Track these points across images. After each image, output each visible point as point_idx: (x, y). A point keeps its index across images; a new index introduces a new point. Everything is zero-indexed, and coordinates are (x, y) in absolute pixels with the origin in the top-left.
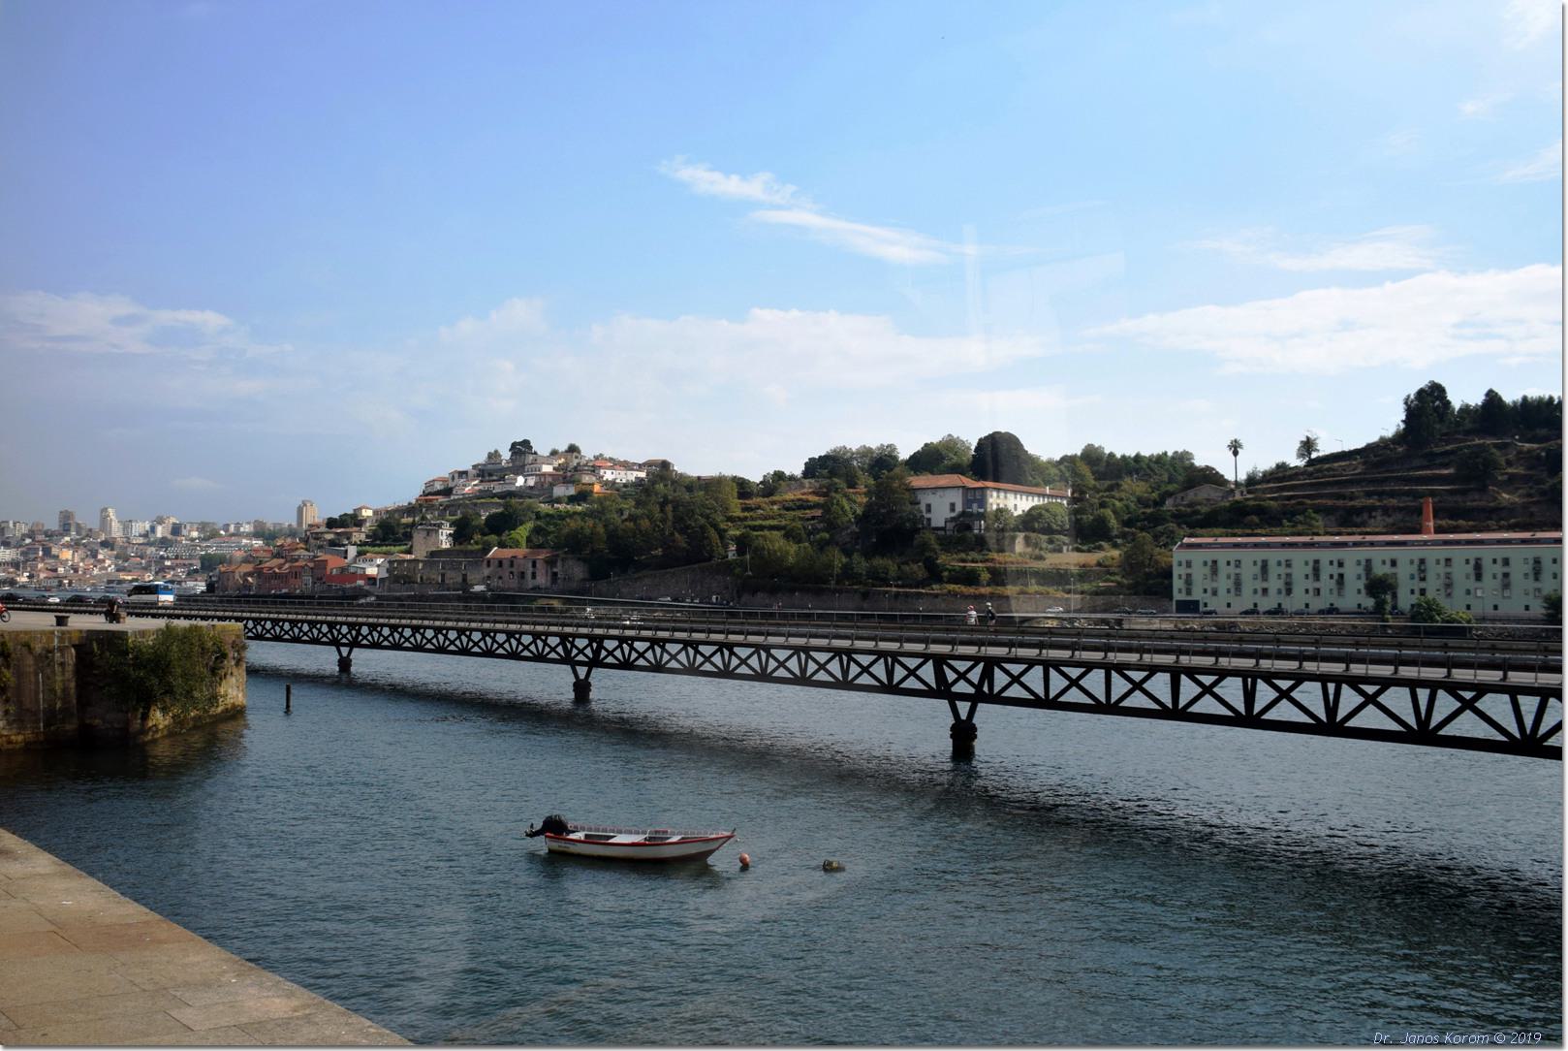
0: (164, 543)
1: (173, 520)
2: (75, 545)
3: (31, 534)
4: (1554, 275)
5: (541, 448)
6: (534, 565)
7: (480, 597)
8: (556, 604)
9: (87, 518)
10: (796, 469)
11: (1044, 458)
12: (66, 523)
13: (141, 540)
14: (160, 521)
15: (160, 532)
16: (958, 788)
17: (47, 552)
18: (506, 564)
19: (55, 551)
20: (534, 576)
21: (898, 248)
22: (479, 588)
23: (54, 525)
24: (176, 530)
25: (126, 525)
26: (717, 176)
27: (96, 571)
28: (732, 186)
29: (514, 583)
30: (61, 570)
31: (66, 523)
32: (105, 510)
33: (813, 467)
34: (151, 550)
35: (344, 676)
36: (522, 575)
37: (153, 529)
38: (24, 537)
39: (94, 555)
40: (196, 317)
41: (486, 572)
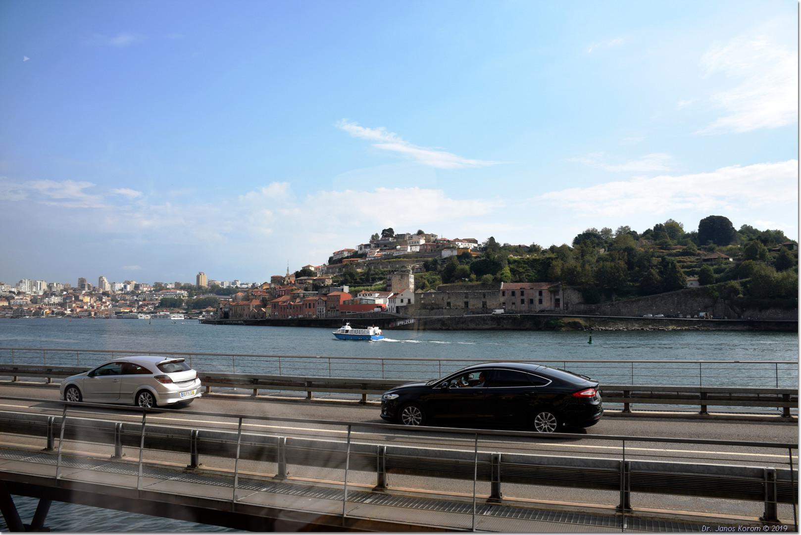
0: (132, 293)
1: (134, 282)
2: (90, 294)
3: (65, 290)
4: (794, 166)
6: (541, 293)
7: (498, 319)
8: (582, 322)
9: (92, 282)
10: (652, 228)
12: (82, 284)
13: (120, 292)
14: (129, 283)
15: (129, 288)
16: (241, 418)
17: (77, 298)
18: (518, 294)
19: (81, 298)
20: (541, 302)
21: (437, 159)
22: (500, 311)
23: (75, 285)
24: (137, 287)
25: (113, 285)
26: (360, 128)
27: (103, 308)
28: (367, 133)
29: (525, 307)
30: (85, 307)
31: (82, 284)
32: (101, 278)
33: (579, 240)
34: (127, 297)
35: (704, 404)
36: (532, 301)
37: (125, 287)
38: (62, 291)
39: (101, 300)
40: (123, 191)
41: (502, 299)
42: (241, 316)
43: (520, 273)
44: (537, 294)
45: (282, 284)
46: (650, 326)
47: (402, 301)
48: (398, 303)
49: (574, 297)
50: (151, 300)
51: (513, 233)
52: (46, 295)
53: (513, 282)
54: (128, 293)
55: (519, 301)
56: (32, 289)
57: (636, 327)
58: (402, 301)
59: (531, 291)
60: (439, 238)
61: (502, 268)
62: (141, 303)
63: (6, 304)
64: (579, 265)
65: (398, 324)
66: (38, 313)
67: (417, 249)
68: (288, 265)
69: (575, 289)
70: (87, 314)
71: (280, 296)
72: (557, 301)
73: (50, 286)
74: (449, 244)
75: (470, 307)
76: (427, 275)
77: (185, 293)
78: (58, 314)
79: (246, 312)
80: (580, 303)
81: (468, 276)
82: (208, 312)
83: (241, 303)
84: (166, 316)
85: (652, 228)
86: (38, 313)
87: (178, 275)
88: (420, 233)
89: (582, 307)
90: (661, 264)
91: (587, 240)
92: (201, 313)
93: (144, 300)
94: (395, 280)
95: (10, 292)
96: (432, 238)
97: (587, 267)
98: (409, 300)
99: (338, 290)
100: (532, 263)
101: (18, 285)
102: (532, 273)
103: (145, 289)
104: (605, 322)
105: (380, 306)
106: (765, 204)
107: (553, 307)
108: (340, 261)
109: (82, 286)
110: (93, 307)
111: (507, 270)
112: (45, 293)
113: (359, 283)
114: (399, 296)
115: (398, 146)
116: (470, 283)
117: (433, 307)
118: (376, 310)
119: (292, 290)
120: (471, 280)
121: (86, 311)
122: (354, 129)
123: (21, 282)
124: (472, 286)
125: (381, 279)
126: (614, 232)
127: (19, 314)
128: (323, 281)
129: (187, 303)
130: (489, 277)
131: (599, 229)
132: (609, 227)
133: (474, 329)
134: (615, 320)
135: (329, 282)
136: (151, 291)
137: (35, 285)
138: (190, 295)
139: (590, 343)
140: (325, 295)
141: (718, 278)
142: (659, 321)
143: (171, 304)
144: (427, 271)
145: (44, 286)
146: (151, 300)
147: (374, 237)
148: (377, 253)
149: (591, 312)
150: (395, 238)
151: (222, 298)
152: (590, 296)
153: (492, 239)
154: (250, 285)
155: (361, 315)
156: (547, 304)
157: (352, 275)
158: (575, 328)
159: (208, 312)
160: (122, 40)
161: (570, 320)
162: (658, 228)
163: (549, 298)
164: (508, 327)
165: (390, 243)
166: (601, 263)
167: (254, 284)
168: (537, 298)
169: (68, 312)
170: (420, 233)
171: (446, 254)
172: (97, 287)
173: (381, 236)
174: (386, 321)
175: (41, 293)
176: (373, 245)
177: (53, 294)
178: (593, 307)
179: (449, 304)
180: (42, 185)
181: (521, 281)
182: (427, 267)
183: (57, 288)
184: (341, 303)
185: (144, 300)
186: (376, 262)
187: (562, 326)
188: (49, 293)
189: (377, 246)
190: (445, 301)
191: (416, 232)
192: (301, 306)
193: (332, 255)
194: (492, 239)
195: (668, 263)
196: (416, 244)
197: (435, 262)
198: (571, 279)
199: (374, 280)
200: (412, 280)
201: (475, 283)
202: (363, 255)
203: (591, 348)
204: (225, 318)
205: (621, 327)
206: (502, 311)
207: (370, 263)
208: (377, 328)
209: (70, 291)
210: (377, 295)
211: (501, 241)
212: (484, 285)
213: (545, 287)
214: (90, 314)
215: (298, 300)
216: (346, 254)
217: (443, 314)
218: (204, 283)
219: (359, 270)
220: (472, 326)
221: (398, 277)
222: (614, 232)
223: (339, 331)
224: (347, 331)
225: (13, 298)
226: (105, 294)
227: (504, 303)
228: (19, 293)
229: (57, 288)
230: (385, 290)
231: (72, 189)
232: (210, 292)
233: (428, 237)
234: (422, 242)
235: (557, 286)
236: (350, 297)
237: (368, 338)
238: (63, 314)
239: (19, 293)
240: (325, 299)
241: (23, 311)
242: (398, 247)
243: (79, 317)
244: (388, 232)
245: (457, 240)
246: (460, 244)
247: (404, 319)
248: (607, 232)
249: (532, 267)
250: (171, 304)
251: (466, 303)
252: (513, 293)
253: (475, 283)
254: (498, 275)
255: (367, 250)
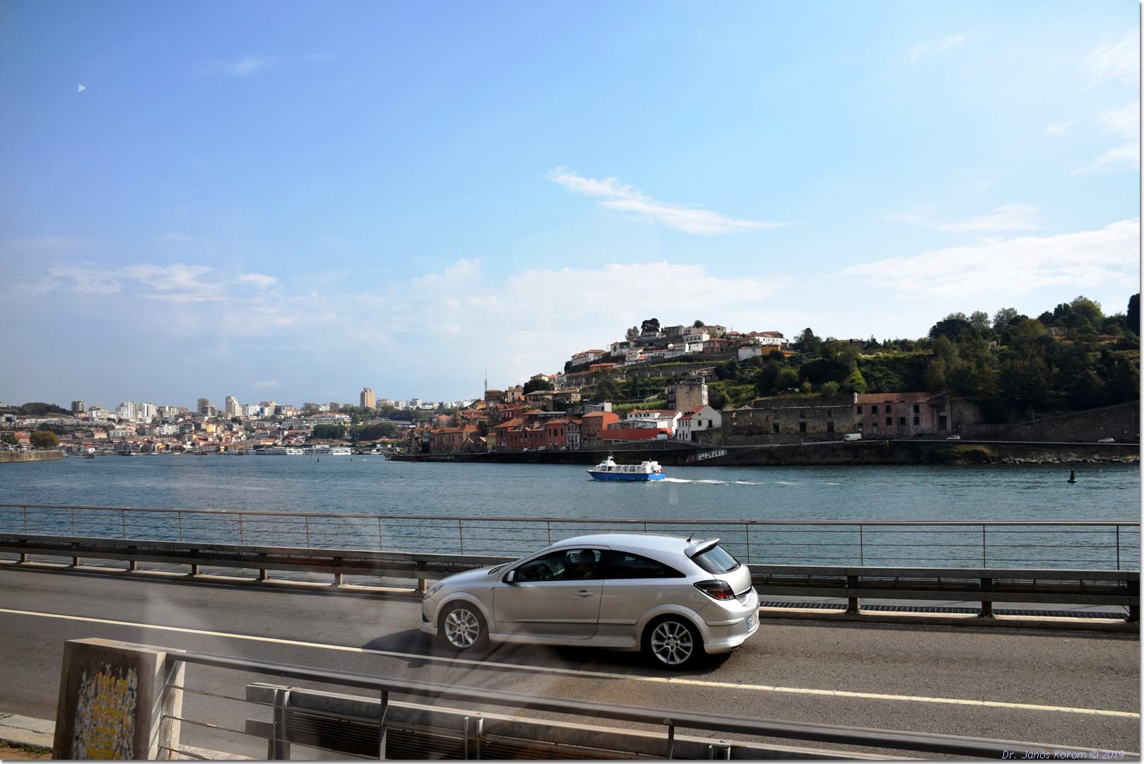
0: (272, 419)
1: (274, 404)
2: (215, 421)
4: (1134, 227)
5: (662, 325)
6: (916, 409)
7: (853, 446)
8: (986, 450)
9: (217, 403)
10: (1052, 311)
11: (1033, 314)
14: (267, 405)
15: (268, 412)
17: (198, 427)
18: (882, 410)
19: (203, 426)
20: (917, 421)
21: (694, 220)
22: (855, 437)
23: (194, 409)
24: (278, 410)
25: (245, 407)
26: (582, 180)
28: (591, 186)
29: (893, 429)
30: (210, 439)
32: (228, 398)
33: (937, 331)
34: (267, 425)
36: (903, 421)
37: (262, 410)
38: (177, 417)
39: (231, 429)
40: (251, 277)
41: (857, 419)
42: (449, 448)
43: (876, 379)
44: (912, 410)
45: (502, 402)
46: (1096, 457)
47: (700, 423)
48: (694, 427)
49: (970, 415)
50: (300, 428)
51: (835, 327)
52: (155, 423)
53: (867, 392)
54: (266, 419)
55: (884, 420)
56: (136, 414)
57: (1074, 457)
58: (700, 423)
59: (902, 406)
60: (728, 331)
61: (849, 372)
62: (286, 433)
63: (104, 436)
64: (973, 365)
65: (700, 458)
66: (147, 449)
67: (700, 348)
68: (512, 378)
69: (968, 401)
70: (214, 448)
71: (509, 419)
72: (942, 419)
73: (160, 411)
74: (747, 340)
75: (809, 430)
76: (721, 385)
77: (346, 418)
78: (174, 449)
79: (457, 442)
80: (977, 423)
81: (799, 384)
82: (384, 444)
83: (447, 430)
84: (327, 451)
85: (1052, 311)
86: (147, 449)
87: (336, 393)
88: (698, 324)
89: (984, 428)
90: (1100, 361)
91: (951, 328)
92: (374, 446)
93: (291, 428)
94: (681, 392)
95: (109, 419)
96: (719, 333)
97: (987, 368)
98: (710, 422)
99: (596, 409)
100: (894, 364)
101: (118, 410)
102: (895, 379)
103: (290, 414)
104: (1023, 450)
105: (662, 432)
106: (1052, 254)
107: (935, 430)
108: (586, 366)
109: (204, 410)
110: (220, 439)
111: (857, 375)
112: (154, 420)
113: (621, 398)
114: (696, 417)
115: (638, 204)
116: (803, 396)
117: (754, 432)
118: (660, 437)
119: (524, 411)
120: (803, 391)
121: (213, 444)
122: (572, 181)
123: (122, 405)
124: (807, 400)
125: (654, 392)
126: (991, 318)
127: (123, 450)
128: (568, 396)
129: (351, 432)
130: (832, 385)
131: (968, 315)
132: (982, 311)
133: (818, 464)
134: (1039, 448)
135: (576, 398)
136: (299, 416)
137: (141, 409)
138: (354, 421)
139: (1071, 481)
140: (579, 416)
141: (1029, 390)
142: (1109, 448)
143: (329, 434)
144: (721, 379)
145: (153, 412)
146: (300, 428)
147: (632, 333)
148: (639, 355)
149: (996, 435)
150: (663, 331)
151: (399, 424)
152: (991, 413)
153: (808, 331)
154: (436, 406)
155: (638, 446)
156: (927, 424)
157: (610, 387)
158: (977, 462)
159: (384, 444)
160: (247, 66)
161: (969, 448)
162: (1062, 310)
163: (929, 416)
164: (871, 460)
165: (658, 340)
166: (1008, 361)
167: (441, 404)
168: (912, 414)
169: (188, 446)
170: (698, 324)
171: (745, 354)
172: (224, 411)
173: (640, 330)
174: (675, 454)
175: (149, 421)
176: (632, 344)
177: (164, 422)
178: (1001, 428)
179: (776, 427)
180: (142, 272)
181: (879, 391)
182: (720, 373)
183: (170, 413)
184: (605, 427)
185: (291, 428)
186: (639, 368)
187: (956, 458)
188: (160, 421)
189: (639, 344)
190: (771, 422)
191: (692, 324)
192: (541, 434)
193: (570, 359)
194: (808, 331)
195: (1113, 360)
196: (696, 340)
197: (732, 366)
198: (961, 386)
199: (644, 394)
200: (705, 393)
201: (810, 395)
202: (621, 359)
203: (1072, 489)
204: (425, 452)
205: (1051, 458)
206: (858, 436)
207: (631, 371)
208: (655, 463)
209: (188, 417)
210: (657, 415)
211: (822, 334)
212: (826, 398)
213: (922, 399)
214: (219, 449)
215: (536, 424)
216: (592, 358)
217: (767, 442)
218: (371, 403)
219: (619, 380)
220: (816, 458)
221: (686, 389)
222: (991, 318)
223: (598, 468)
224: (610, 468)
225: (113, 428)
226: (235, 420)
227: (860, 425)
228: (121, 421)
229: (170, 413)
230: (668, 407)
231: (182, 276)
232: (382, 416)
233: (711, 330)
234: (706, 337)
235: (941, 398)
236: (616, 419)
237: (644, 478)
238: (181, 449)
239: (121, 421)
240: (579, 422)
241: (126, 446)
242: (671, 346)
243: (204, 453)
244: (651, 325)
245: (754, 334)
246: (761, 339)
247: (709, 450)
248: (980, 317)
249: (894, 369)
250: (329, 434)
251: (803, 426)
252: (874, 409)
253: (810, 395)
254: (847, 383)
255: (625, 351)
